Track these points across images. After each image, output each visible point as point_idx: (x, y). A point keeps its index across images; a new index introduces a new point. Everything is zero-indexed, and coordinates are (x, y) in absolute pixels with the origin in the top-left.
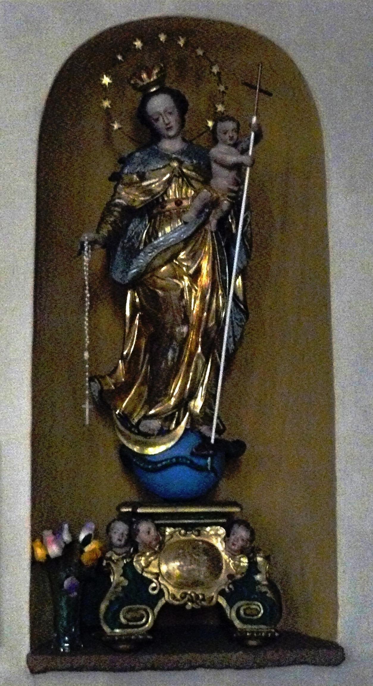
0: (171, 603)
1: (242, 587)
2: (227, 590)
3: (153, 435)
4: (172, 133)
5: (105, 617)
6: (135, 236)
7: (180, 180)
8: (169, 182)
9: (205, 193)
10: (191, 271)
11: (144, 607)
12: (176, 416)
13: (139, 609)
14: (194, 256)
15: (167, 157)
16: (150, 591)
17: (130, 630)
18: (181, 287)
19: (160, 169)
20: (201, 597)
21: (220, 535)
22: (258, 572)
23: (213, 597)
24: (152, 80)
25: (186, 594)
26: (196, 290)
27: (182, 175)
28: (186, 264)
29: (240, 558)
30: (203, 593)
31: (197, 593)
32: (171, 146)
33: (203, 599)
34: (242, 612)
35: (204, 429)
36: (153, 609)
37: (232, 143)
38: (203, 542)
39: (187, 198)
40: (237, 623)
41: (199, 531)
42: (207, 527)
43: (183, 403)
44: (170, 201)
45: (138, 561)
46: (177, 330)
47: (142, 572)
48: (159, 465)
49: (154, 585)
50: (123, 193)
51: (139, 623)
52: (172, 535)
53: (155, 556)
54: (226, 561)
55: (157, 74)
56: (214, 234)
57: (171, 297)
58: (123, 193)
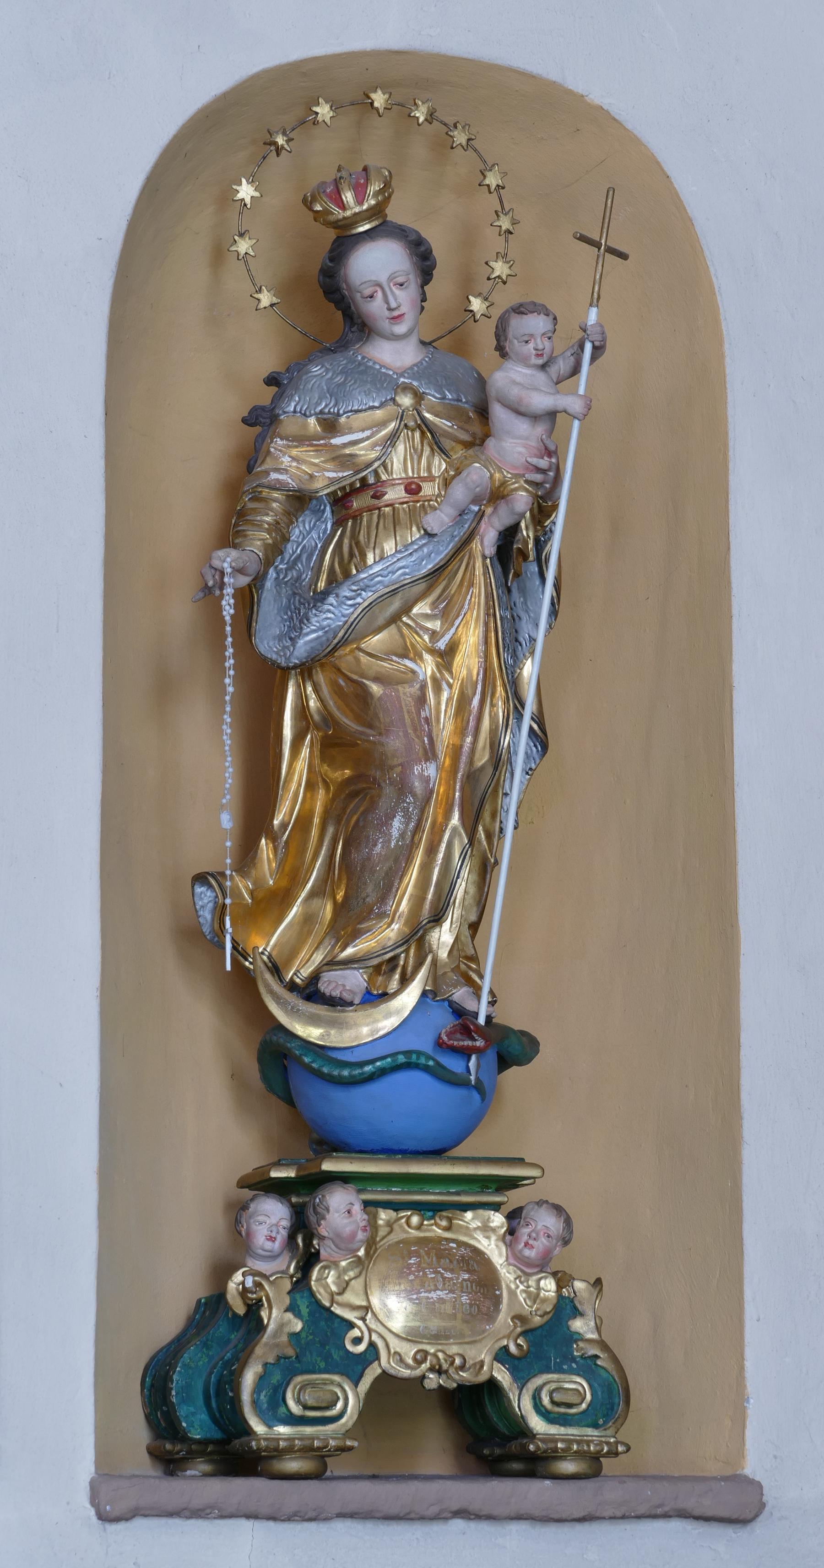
0: (392, 1372)
1: (546, 1342)
2: (513, 1349)
3: (351, 1004)
4: (400, 329)
5: (255, 1403)
6: (304, 557)
7: (417, 435)
8: (392, 439)
9: (477, 474)
10: (442, 645)
11: (336, 1378)
12: (402, 963)
13: (325, 1382)
14: (447, 612)
15: (387, 383)
16: (350, 1347)
17: (308, 1430)
18: (421, 678)
19: (372, 408)
20: (458, 1361)
21: (494, 1230)
22: (577, 1313)
23: (482, 1364)
24: (365, 207)
25: (426, 1353)
26: (450, 686)
27: (424, 427)
28: (429, 625)
29: (540, 1279)
30: (461, 1352)
31: (449, 1352)
32: (396, 354)
33: (462, 1367)
34: (546, 1400)
35: (460, 995)
36: (356, 1383)
37: (540, 362)
38: (460, 1244)
39: (431, 478)
40: (537, 1424)
41: (450, 1220)
42: (465, 1211)
43: (417, 936)
44: (392, 483)
45: (321, 1279)
46: (417, 769)
47: (332, 1305)
48: (368, 1069)
49: (356, 1333)
50: (286, 460)
51: (328, 1413)
52: (390, 1224)
53: (357, 1270)
54: (508, 1287)
55: (376, 194)
56: (488, 561)
57: (398, 698)
58: (286, 460)
